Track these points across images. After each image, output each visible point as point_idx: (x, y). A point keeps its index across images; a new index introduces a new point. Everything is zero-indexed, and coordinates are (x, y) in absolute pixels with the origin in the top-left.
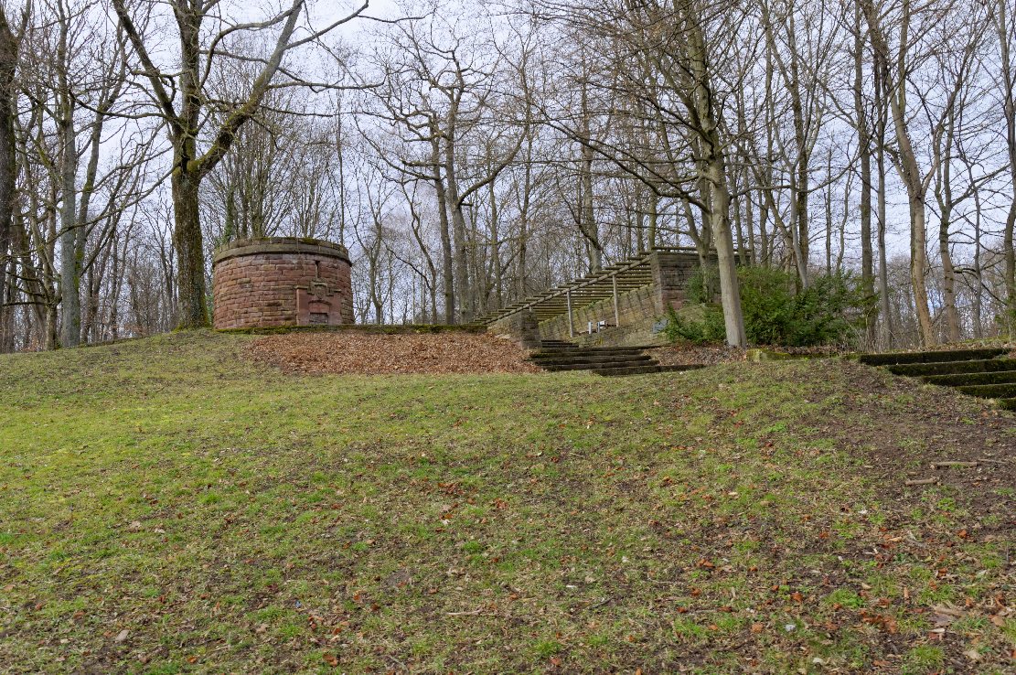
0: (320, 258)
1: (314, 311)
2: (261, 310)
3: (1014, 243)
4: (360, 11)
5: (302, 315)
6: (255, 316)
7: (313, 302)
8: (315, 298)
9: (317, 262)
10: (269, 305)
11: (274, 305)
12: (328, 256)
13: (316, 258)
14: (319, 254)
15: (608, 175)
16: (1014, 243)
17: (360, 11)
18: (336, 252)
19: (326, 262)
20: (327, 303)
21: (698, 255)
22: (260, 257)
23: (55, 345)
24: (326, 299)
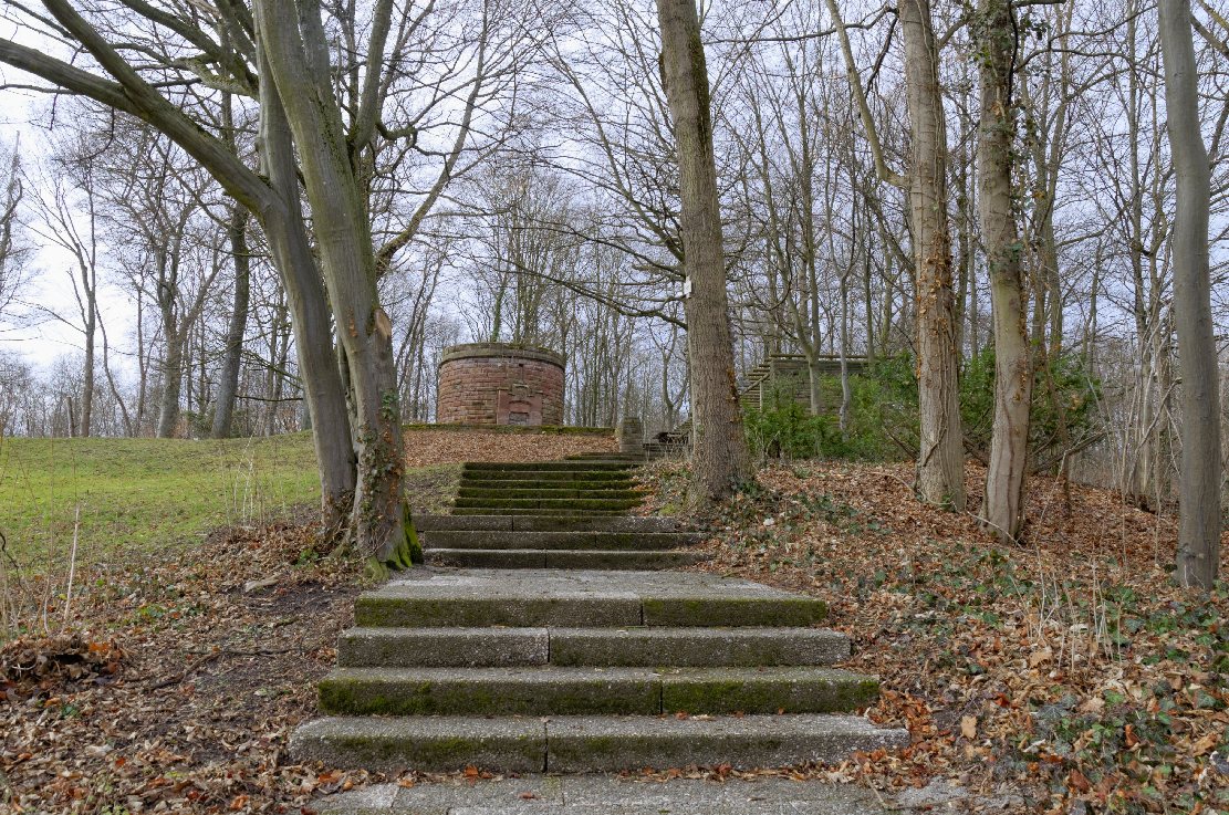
0: (524, 361)
1: (515, 410)
2: (467, 409)
3: (1224, 496)
4: (455, 90)
5: (502, 414)
6: (463, 415)
7: (513, 402)
8: (515, 399)
9: (521, 365)
10: (474, 404)
11: (478, 405)
12: (532, 359)
13: (520, 361)
14: (522, 358)
15: (773, 289)
16: (1224, 496)
17: (455, 90)
18: (541, 356)
19: (530, 365)
20: (528, 403)
21: (839, 362)
22: (470, 360)
23: (169, 433)
24: (528, 400)
